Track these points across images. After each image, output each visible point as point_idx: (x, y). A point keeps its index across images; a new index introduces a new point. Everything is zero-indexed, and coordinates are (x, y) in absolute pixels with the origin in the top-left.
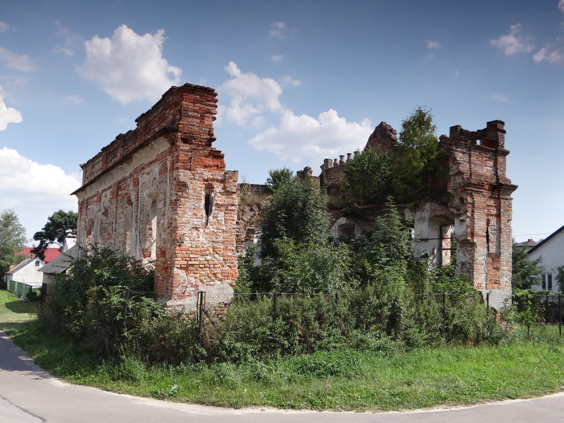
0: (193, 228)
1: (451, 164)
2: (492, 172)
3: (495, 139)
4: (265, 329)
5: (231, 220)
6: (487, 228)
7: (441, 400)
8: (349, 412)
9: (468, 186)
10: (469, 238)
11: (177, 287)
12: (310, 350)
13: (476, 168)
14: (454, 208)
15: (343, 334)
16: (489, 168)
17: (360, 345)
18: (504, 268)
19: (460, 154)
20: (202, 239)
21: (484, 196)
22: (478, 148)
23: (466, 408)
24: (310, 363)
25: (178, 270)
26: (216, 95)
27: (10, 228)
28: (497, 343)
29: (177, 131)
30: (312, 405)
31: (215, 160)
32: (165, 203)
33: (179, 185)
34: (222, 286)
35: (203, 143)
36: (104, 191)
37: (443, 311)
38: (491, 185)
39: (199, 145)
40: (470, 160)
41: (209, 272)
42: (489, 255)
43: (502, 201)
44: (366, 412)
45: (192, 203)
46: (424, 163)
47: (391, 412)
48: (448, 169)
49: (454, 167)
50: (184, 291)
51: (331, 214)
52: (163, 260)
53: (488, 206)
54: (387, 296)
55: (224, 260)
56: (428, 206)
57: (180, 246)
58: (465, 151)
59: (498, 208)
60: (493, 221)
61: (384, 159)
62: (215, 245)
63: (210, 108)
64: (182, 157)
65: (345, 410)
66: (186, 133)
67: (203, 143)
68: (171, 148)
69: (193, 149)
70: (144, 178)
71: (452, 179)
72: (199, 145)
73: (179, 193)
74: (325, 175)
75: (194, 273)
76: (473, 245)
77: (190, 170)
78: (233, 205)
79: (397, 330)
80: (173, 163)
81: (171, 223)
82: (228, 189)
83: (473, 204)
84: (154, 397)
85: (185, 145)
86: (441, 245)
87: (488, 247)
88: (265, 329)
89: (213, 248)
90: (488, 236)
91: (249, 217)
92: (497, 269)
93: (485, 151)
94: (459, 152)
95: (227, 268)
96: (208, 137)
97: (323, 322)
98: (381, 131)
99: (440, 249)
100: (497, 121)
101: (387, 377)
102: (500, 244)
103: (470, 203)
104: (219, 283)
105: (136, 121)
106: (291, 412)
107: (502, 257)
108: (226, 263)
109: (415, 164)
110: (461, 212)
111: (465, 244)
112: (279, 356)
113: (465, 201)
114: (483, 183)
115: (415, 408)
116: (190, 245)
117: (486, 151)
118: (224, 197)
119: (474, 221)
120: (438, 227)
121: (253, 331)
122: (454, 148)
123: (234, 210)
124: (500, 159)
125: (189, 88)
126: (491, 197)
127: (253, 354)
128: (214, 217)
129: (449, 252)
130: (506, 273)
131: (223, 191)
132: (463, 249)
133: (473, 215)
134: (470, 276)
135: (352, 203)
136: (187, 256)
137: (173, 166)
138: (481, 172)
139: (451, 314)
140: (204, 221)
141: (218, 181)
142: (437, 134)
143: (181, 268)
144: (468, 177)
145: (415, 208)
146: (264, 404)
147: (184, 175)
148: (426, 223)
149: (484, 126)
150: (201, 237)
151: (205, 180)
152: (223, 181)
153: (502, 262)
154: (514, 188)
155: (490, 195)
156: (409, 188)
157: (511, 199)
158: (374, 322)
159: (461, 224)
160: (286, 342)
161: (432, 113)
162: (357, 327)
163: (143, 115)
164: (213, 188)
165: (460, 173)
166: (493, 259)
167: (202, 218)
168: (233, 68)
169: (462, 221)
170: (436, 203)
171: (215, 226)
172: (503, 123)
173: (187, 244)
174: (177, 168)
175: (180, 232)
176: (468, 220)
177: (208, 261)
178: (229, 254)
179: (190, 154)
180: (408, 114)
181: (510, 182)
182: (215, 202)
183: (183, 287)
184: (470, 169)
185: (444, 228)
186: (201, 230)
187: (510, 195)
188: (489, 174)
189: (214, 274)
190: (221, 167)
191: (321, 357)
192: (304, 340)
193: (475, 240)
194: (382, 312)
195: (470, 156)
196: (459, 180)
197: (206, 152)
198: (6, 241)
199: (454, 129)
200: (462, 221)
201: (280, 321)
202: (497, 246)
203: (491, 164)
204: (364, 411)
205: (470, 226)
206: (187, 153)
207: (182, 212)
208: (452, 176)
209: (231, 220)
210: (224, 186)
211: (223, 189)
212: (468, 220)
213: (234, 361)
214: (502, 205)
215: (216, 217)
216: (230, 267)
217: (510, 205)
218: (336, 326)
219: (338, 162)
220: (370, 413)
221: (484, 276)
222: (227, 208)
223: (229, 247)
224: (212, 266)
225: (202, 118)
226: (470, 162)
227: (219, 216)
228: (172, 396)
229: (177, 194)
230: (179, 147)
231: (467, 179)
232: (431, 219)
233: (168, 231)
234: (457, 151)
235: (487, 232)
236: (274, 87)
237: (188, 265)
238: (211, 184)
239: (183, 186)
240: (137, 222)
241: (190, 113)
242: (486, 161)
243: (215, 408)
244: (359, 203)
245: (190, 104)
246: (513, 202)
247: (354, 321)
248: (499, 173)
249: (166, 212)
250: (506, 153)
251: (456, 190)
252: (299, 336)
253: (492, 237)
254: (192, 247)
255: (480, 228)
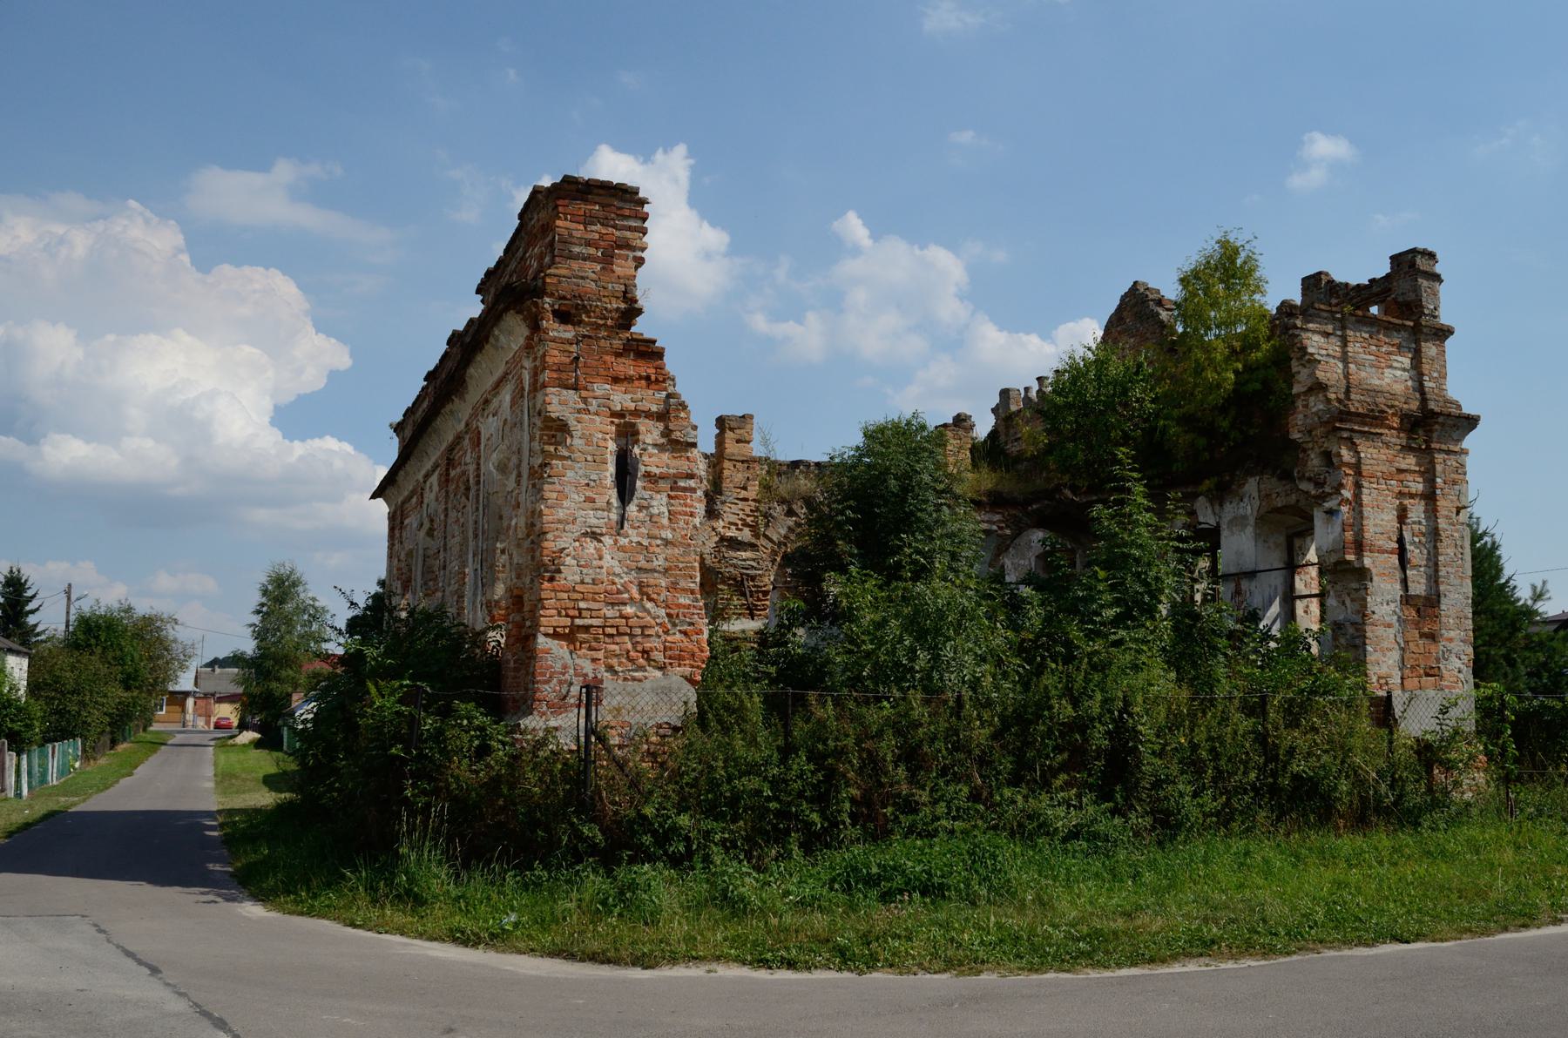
0: (585, 534)
1: (1295, 366)
2: (1410, 383)
3: (1411, 296)
4: (752, 783)
5: (685, 514)
6: (1401, 530)
7: (1204, 947)
8: (936, 976)
9: (1341, 421)
10: (1350, 557)
11: (547, 682)
12: (879, 834)
13: (1363, 374)
14: (1310, 479)
15: (975, 796)
16: (1399, 373)
17: (1029, 830)
18: (1452, 634)
19: (1316, 338)
20: (610, 561)
21: (1387, 445)
22: (1373, 321)
23: (1263, 963)
24: (868, 867)
25: (549, 640)
26: (643, 202)
27: (289, 607)
28: (1417, 824)
29: (541, 292)
30: (844, 958)
31: (641, 362)
32: (519, 475)
33: (550, 428)
34: (665, 683)
35: (609, 322)
36: (427, 476)
37: (1261, 739)
38: (1405, 417)
39: (598, 327)
40: (1345, 353)
41: (629, 646)
42: (1407, 599)
43: (1439, 457)
44: (983, 976)
45: (581, 472)
46: (1236, 372)
47: (1051, 975)
48: (1290, 378)
49: (1305, 372)
50: (564, 692)
51: (997, 517)
52: (518, 618)
53: (1400, 471)
54: (1099, 696)
55: (669, 615)
56: (1251, 486)
57: (552, 579)
58: (1329, 328)
59: (1429, 475)
60: (1417, 511)
61: (1137, 373)
62: (644, 577)
63: (628, 234)
64: (555, 356)
65: (927, 970)
66: (564, 298)
67: (609, 322)
68: (529, 338)
69: (584, 336)
70: (489, 426)
71: (1299, 404)
72: (598, 327)
73: (547, 447)
74: (1001, 429)
75: (591, 649)
76: (1363, 574)
77: (575, 388)
78: (691, 476)
79: (1131, 790)
80: (535, 374)
81: (533, 525)
82: (676, 435)
83: (1357, 467)
84: (455, 940)
85: (562, 327)
86: (1292, 586)
87: (1404, 582)
88: (752, 783)
89: (641, 586)
90: (1402, 552)
91: (783, 532)
92: (1432, 637)
93: (1386, 328)
94: (1314, 332)
95: (678, 636)
96: (623, 306)
97: (921, 768)
98: (1135, 305)
99: (1290, 598)
100: (1414, 251)
101: (1081, 899)
102: (1437, 571)
103: (1348, 465)
104: (659, 674)
105: (478, 292)
106: (785, 975)
107: (1445, 604)
108: (674, 625)
109: (1210, 375)
110: (1328, 489)
111: (1345, 575)
112: (796, 852)
113: (1335, 460)
114: (1382, 412)
115: (1119, 965)
116: (578, 578)
117: (1388, 328)
118: (666, 456)
119: (1361, 512)
120: (1282, 539)
121: (725, 787)
122: (1299, 323)
123: (694, 490)
124: (1430, 349)
125: (573, 187)
126: (1407, 449)
127: (728, 846)
128: (641, 508)
129: (1314, 606)
130: (1457, 646)
131: (663, 440)
132: (1338, 587)
133: (1357, 496)
134: (1356, 659)
135: (1058, 489)
136: (571, 604)
137: (536, 381)
138: (1378, 382)
139: (1285, 744)
140: (614, 517)
141: (648, 415)
142: (1271, 303)
143: (555, 635)
144: (1342, 396)
145: (1221, 494)
146: (718, 958)
147: (559, 403)
148: (1250, 530)
149: (1382, 269)
150: (607, 557)
151: (614, 414)
152: (662, 416)
153: (1444, 619)
154: (1471, 422)
155: (1404, 442)
156: (1202, 442)
157: (1465, 452)
158: (1064, 767)
159: (1328, 522)
160: (815, 817)
161: (1258, 247)
162: (1015, 781)
163: (489, 273)
164: (637, 433)
165: (1319, 387)
166: (1418, 611)
167: (609, 511)
168: (854, 227)
169: (1331, 513)
170: (1273, 475)
171: (643, 530)
172: (1431, 256)
173: (570, 574)
174: (544, 386)
175: (550, 545)
176: (1344, 509)
177: (627, 618)
178: (682, 601)
179: (574, 348)
180: (1193, 250)
181: (1459, 407)
182: (642, 469)
183: (560, 682)
184: (1347, 375)
185: (1297, 542)
186: (608, 540)
187: (1460, 440)
188: (1399, 388)
189: (644, 652)
190: (657, 380)
191: (903, 854)
192: (865, 812)
193: (1367, 562)
194: (1086, 740)
195: (1345, 342)
196: (1317, 405)
197: (617, 343)
198: (282, 637)
199: (1312, 283)
200: (1331, 513)
201: (800, 762)
202: (1429, 578)
203: (1406, 361)
204: (980, 972)
205: (1352, 525)
206: (567, 347)
207: (555, 495)
208: (1298, 395)
209: (685, 514)
210: (666, 427)
211: (663, 435)
212: (1344, 509)
213: (676, 861)
214: (1439, 468)
215: (647, 508)
216: (685, 633)
217: (1461, 469)
218: (957, 779)
219: (1033, 394)
220: (995, 976)
221: (1395, 655)
222: (674, 484)
223: (683, 584)
224: (639, 631)
225: (607, 260)
226: (1345, 359)
227: (654, 503)
228: (497, 939)
229: (543, 451)
230: (546, 331)
231: (1339, 401)
232: (1261, 520)
233: (527, 544)
234: (1307, 330)
235: (1401, 540)
236: (947, 265)
237: (574, 629)
238: (633, 425)
239: (558, 430)
240: (476, 536)
241: (576, 249)
242: (1389, 353)
243: (597, 966)
244: (1074, 490)
245: (574, 225)
246: (1469, 461)
247: (1006, 765)
248: (1428, 384)
249: (522, 498)
250: (1443, 333)
251: (1310, 432)
252: (853, 800)
253: (1416, 554)
254: (582, 582)
255: (1379, 530)
